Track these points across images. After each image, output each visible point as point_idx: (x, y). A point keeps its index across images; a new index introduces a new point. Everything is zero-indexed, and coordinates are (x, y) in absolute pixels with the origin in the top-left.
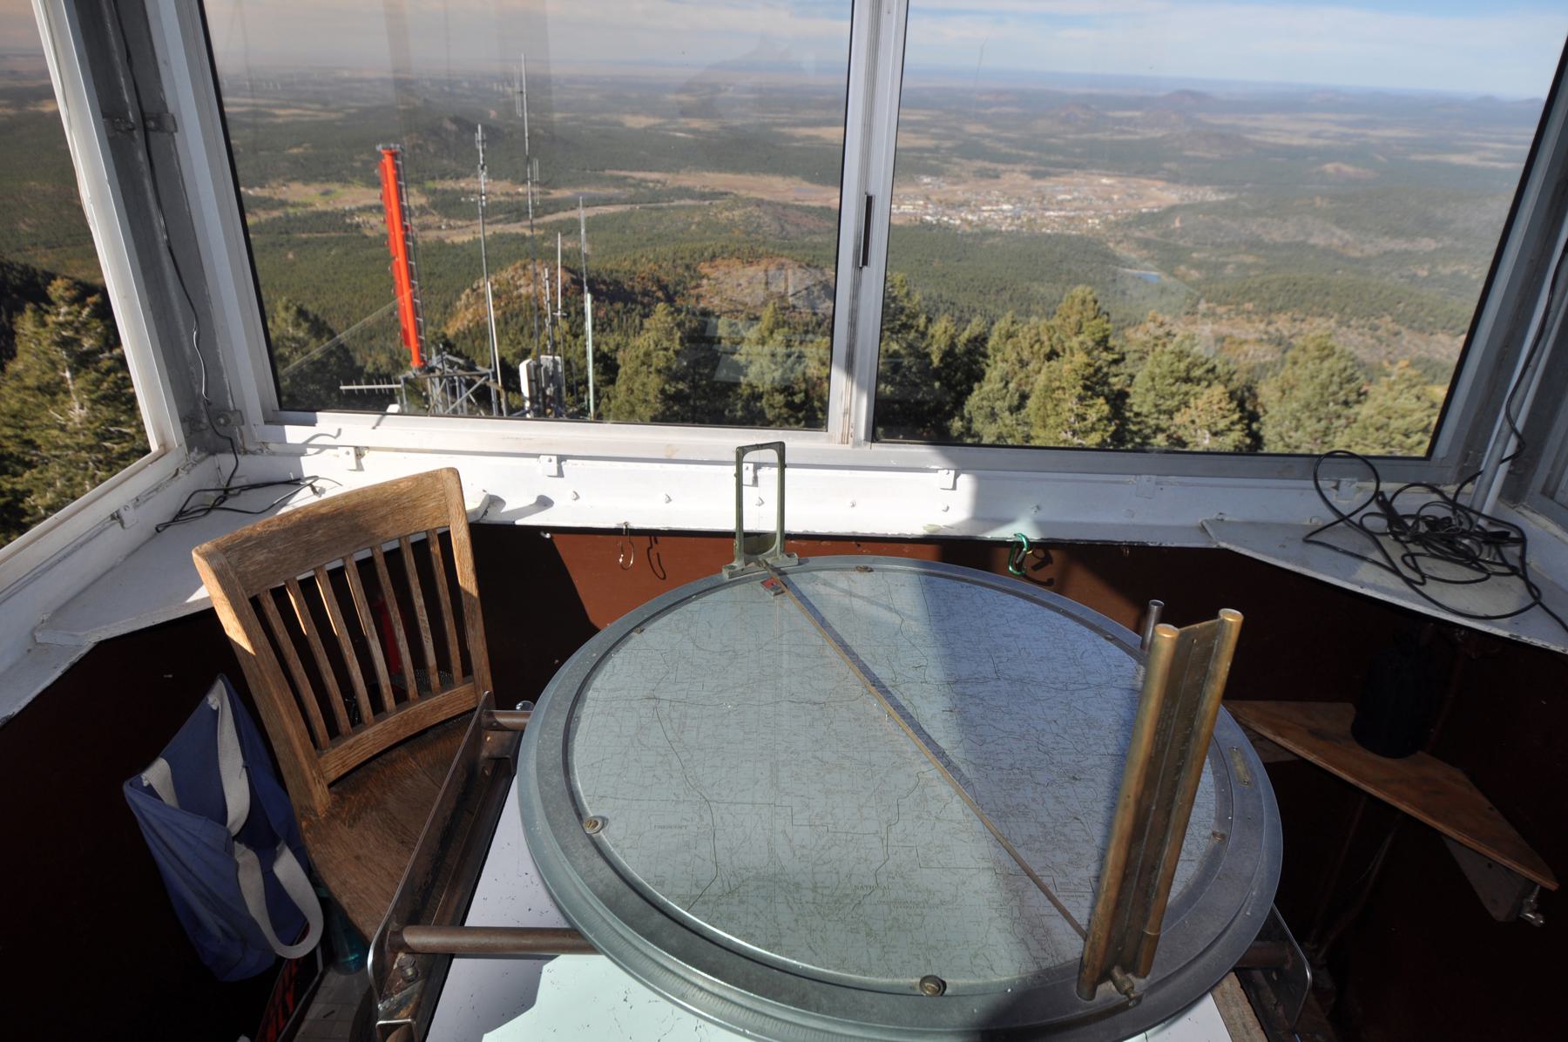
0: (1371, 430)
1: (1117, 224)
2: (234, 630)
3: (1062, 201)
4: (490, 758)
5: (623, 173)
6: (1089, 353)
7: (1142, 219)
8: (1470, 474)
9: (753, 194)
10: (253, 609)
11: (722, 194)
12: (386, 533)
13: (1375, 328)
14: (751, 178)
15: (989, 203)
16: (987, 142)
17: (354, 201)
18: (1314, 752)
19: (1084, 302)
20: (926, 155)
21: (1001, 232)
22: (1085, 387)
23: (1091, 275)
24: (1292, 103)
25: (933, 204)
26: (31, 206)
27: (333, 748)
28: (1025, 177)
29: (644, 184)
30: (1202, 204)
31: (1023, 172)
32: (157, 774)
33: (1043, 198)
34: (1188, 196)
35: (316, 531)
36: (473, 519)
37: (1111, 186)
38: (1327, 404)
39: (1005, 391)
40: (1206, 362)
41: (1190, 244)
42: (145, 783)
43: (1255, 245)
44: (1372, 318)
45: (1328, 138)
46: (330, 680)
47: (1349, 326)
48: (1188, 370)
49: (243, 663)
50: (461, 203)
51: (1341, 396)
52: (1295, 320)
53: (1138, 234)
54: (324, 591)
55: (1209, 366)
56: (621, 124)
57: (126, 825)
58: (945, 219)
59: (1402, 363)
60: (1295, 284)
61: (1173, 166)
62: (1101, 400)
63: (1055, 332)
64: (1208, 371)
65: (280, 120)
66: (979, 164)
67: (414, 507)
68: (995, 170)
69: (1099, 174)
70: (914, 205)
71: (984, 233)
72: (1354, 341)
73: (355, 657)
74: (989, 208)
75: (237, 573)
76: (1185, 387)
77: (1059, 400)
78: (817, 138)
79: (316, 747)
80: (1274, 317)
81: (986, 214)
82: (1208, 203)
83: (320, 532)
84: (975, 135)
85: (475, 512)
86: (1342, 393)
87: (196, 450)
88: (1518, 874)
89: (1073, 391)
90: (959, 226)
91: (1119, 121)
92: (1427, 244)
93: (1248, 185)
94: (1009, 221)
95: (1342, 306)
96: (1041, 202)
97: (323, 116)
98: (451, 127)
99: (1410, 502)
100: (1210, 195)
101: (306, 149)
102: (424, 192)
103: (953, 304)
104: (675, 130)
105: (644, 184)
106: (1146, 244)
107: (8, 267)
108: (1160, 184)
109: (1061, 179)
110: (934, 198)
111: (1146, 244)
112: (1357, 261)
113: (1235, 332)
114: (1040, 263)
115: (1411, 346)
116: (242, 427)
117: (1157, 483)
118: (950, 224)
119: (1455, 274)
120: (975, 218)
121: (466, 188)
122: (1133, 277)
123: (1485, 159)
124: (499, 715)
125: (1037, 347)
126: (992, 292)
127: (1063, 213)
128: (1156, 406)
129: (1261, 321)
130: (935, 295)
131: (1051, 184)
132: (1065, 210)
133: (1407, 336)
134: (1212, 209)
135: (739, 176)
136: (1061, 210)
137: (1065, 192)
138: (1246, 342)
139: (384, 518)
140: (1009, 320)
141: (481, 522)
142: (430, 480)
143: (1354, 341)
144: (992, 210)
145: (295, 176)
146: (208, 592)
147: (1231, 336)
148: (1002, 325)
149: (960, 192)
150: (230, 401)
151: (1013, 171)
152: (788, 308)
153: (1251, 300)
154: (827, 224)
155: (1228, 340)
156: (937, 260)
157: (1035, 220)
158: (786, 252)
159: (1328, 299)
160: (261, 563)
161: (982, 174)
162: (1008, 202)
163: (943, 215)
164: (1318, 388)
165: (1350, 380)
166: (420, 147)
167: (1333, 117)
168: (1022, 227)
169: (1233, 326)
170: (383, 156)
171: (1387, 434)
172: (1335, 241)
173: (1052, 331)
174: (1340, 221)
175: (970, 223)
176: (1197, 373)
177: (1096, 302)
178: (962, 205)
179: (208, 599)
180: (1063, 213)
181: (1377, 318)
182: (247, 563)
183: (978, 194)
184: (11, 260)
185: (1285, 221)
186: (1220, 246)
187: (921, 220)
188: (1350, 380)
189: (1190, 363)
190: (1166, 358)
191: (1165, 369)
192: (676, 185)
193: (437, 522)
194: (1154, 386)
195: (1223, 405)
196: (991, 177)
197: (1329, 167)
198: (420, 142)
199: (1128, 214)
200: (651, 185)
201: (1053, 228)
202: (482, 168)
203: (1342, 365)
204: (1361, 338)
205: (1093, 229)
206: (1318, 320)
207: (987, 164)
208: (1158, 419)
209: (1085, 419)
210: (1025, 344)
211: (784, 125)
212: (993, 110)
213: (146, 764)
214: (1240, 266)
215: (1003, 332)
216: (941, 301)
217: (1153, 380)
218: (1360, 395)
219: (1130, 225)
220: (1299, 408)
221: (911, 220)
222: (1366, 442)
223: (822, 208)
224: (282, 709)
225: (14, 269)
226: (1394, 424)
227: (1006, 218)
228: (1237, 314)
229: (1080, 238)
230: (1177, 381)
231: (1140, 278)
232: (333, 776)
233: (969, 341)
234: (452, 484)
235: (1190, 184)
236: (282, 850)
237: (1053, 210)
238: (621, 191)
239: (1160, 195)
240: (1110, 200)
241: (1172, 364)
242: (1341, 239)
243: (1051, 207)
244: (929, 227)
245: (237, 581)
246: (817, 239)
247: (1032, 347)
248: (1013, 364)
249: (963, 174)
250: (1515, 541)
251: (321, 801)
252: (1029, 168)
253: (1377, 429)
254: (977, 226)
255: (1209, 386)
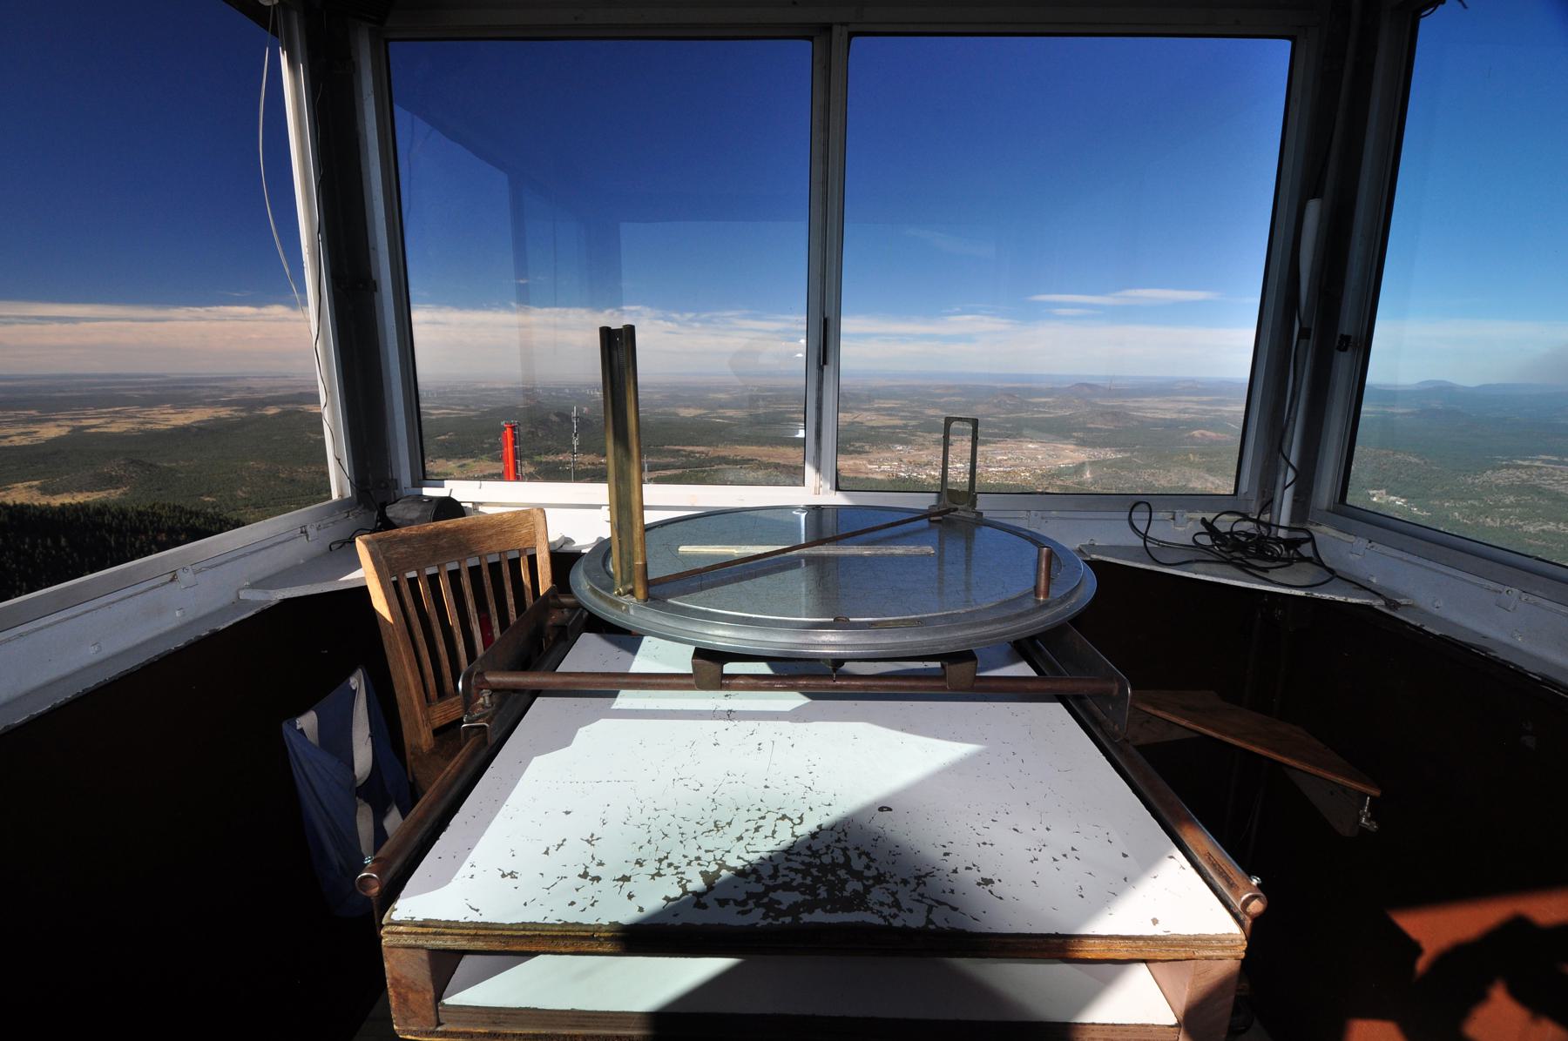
1: (1043, 476)
2: (380, 604)
4: (554, 626)
5: (677, 448)
8: (1268, 504)
9: (772, 460)
10: (394, 591)
11: (749, 460)
12: (491, 547)
14: (771, 449)
17: (481, 471)
18: (1186, 718)
20: (898, 430)
24: (1165, 390)
26: (248, 479)
27: (440, 702)
29: (692, 455)
32: (308, 722)
35: (442, 539)
36: (552, 548)
37: (1035, 449)
42: (298, 727)
45: (1192, 413)
46: (442, 649)
49: (381, 624)
50: (559, 471)
54: (444, 584)
56: (677, 415)
57: (278, 753)
58: (915, 475)
61: (1080, 435)
65: (434, 417)
67: (512, 532)
73: (461, 635)
75: (384, 557)
79: (427, 701)
83: (445, 540)
84: (933, 416)
85: (554, 543)
87: (362, 505)
88: (1349, 788)
90: (925, 479)
91: (1037, 405)
93: (1137, 447)
94: (962, 475)
97: (465, 414)
98: (554, 418)
99: (1224, 524)
101: (451, 436)
102: (532, 464)
104: (716, 418)
105: (692, 455)
107: (225, 522)
108: (1072, 447)
109: (998, 445)
110: (905, 460)
116: (396, 491)
117: (1042, 518)
121: (564, 460)
124: (562, 597)
135: (762, 448)
137: (1001, 454)
139: (490, 537)
141: (559, 551)
142: (525, 514)
145: (441, 455)
146: (366, 574)
150: (390, 473)
160: (402, 553)
163: (913, 471)
166: (532, 433)
167: (1195, 399)
170: (505, 429)
172: (1209, 485)
174: (1210, 470)
178: (927, 465)
179: (364, 579)
182: (393, 552)
184: (228, 516)
185: (1169, 471)
187: (897, 475)
192: (716, 455)
193: (528, 544)
197: (1196, 433)
198: (533, 430)
200: (698, 455)
202: (576, 435)
205: (1025, 479)
211: (794, 412)
212: (945, 399)
213: (301, 712)
219: (1053, 476)
224: (405, 662)
225: (228, 523)
232: (437, 724)
234: (539, 518)
236: (393, 807)
237: (995, 467)
238: (676, 460)
245: (384, 562)
249: (926, 443)
250: (1306, 541)
251: (426, 741)
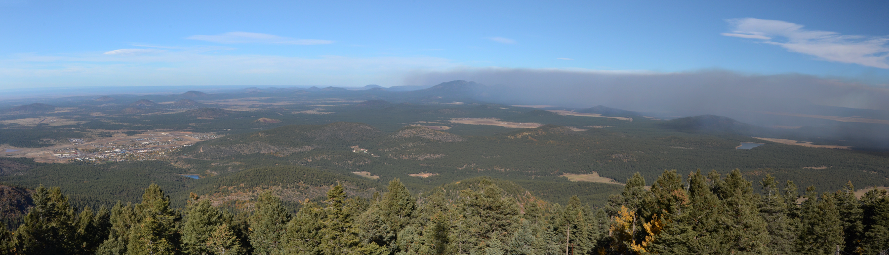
0: (294, 233)
1: (173, 153)
3: (145, 145)
6: (154, 217)
7: (185, 150)
13: (298, 187)
15: (109, 149)
16: (103, 120)
19: (155, 192)
21: (117, 162)
22: (154, 234)
23: (165, 179)
25: (79, 152)
28: (125, 135)
30: (210, 140)
31: (123, 133)
33: (135, 145)
34: (204, 137)
37: (166, 136)
38: (276, 224)
39: (116, 242)
40: (217, 213)
41: (209, 160)
43: (238, 157)
44: (296, 183)
47: (287, 188)
48: (209, 218)
51: (280, 219)
52: (264, 189)
53: (184, 157)
55: (219, 215)
59: (307, 200)
60: (260, 172)
61: (194, 124)
62: (164, 240)
63: (143, 209)
64: (219, 218)
66: (100, 131)
68: (109, 133)
69: (160, 131)
70: (70, 153)
71: (108, 165)
72: (291, 194)
74: (109, 151)
76: (209, 227)
77: (144, 243)
78: (16, 124)
80: (255, 188)
81: (108, 154)
82: (213, 140)
84: (96, 117)
86: (280, 218)
89: (148, 237)
90: (95, 161)
92: (308, 148)
94: (120, 157)
95: (282, 179)
96: (135, 146)
100: (213, 136)
103: (98, 201)
106: (189, 161)
110: (80, 149)
111: (189, 161)
112: (283, 158)
113: (239, 198)
114: (139, 176)
115: (314, 193)
118: (90, 161)
119: (322, 159)
120: (103, 157)
122: (186, 178)
123: (320, 111)
125: (133, 217)
126: (117, 193)
127: (146, 151)
128: (198, 239)
129: (250, 191)
130: (87, 198)
131: (138, 137)
132: (147, 149)
133: (311, 188)
134: (216, 142)
136: (145, 149)
137: (145, 141)
138: (245, 202)
140: (119, 205)
143: (291, 194)
144: (111, 152)
147: (238, 200)
148: (116, 208)
149: (93, 145)
151: (118, 133)
152: (8, 211)
153: (242, 182)
154: (25, 166)
155: (237, 202)
156: (86, 180)
157: (133, 155)
158: (4, 182)
159: (275, 177)
161: (102, 135)
162: (118, 147)
163: (86, 157)
164: (269, 217)
165: (282, 211)
168: (127, 159)
169: (237, 195)
171: (301, 233)
172: (272, 151)
173: (142, 208)
175: (100, 159)
176: (213, 219)
177: (161, 191)
180: (146, 151)
181: (297, 183)
183: (102, 145)
185: (248, 144)
186: (223, 159)
187: (75, 160)
188: (282, 211)
189: (209, 215)
190: (197, 214)
191: (198, 220)
194: (194, 229)
195: (227, 233)
196: (107, 136)
197: (261, 120)
199: (178, 148)
201: (143, 158)
203: (276, 205)
204: (293, 193)
206: (274, 187)
207: (104, 131)
208: (200, 245)
209: (158, 251)
210: (127, 217)
212: (104, 105)
214: (234, 167)
215: (117, 212)
216: (91, 200)
217: (193, 226)
218: (288, 217)
220: (240, 228)
221: (69, 161)
222: (295, 239)
223: (22, 158)
226: (303, 228)
227: (118, 155)
228: (238, 190)
229: (157, 162)
230: (205, 225)
231: (190, 178)
233: (100, 218)
235: (203, 132)
237: (141, 150)
239: (191, 138)
240: (168, 142)
241: (201, 217)
242: (274, 150)
243: (140, 148)
244: (80, 163)
246: (21, 174)
247: (130, 218)
248: (122, 228)
252: (126, 131)
253: (297, 232)
254: (104, 160)
255: (221, 224)
